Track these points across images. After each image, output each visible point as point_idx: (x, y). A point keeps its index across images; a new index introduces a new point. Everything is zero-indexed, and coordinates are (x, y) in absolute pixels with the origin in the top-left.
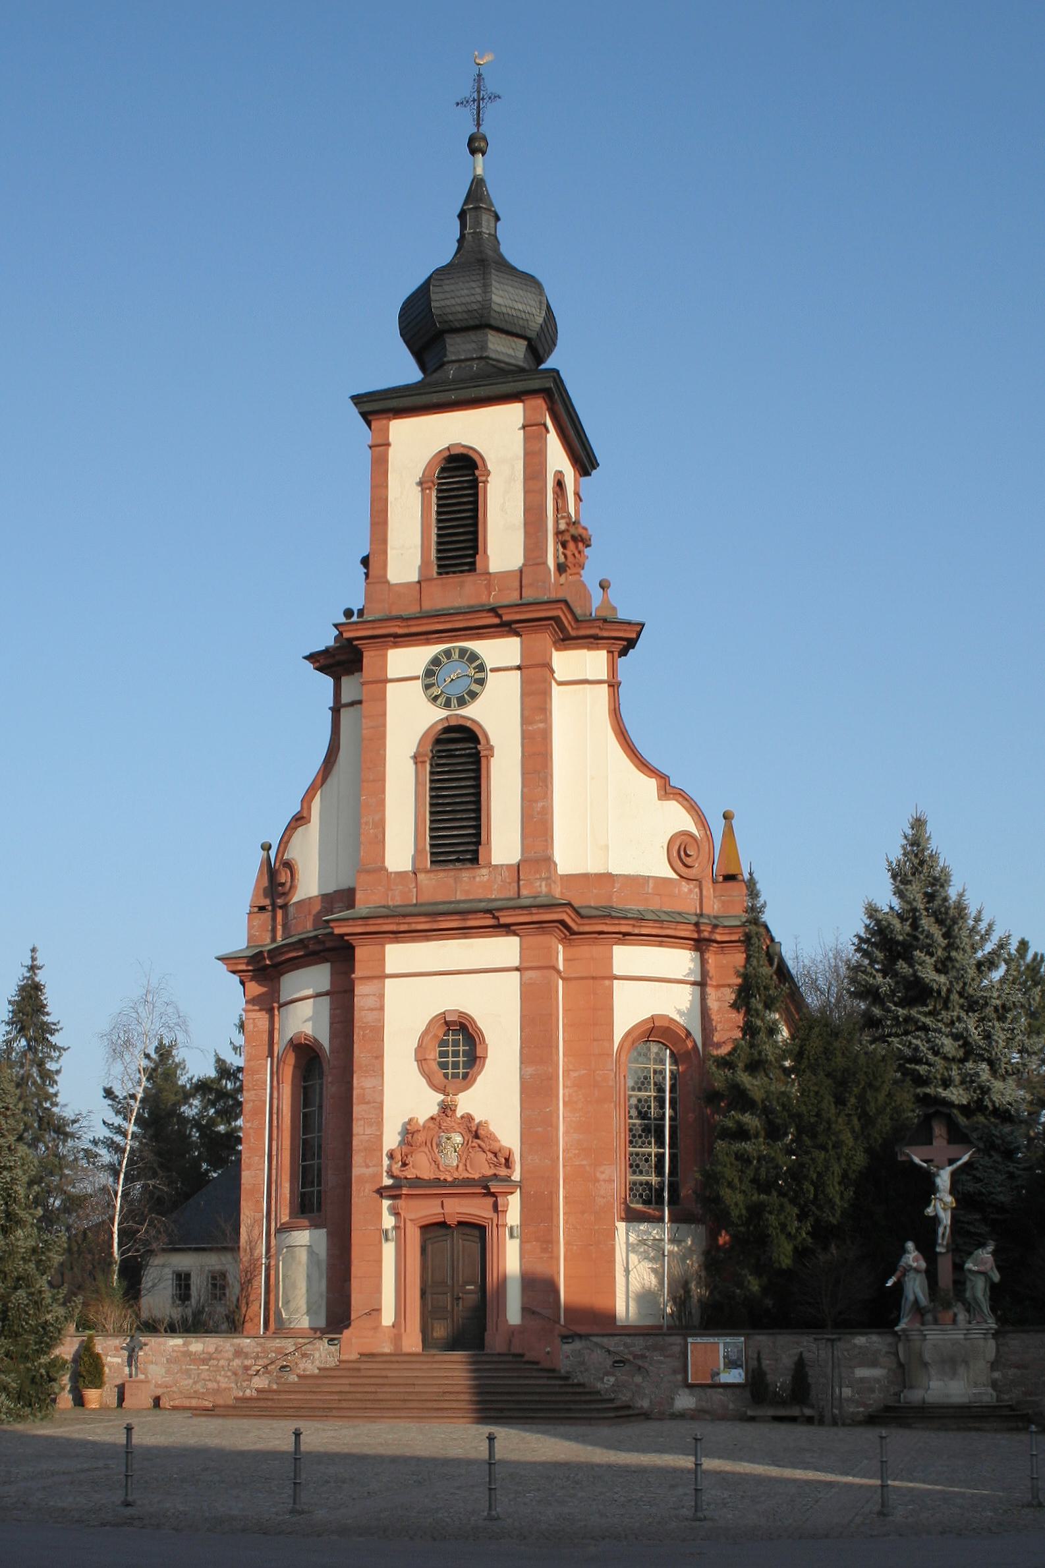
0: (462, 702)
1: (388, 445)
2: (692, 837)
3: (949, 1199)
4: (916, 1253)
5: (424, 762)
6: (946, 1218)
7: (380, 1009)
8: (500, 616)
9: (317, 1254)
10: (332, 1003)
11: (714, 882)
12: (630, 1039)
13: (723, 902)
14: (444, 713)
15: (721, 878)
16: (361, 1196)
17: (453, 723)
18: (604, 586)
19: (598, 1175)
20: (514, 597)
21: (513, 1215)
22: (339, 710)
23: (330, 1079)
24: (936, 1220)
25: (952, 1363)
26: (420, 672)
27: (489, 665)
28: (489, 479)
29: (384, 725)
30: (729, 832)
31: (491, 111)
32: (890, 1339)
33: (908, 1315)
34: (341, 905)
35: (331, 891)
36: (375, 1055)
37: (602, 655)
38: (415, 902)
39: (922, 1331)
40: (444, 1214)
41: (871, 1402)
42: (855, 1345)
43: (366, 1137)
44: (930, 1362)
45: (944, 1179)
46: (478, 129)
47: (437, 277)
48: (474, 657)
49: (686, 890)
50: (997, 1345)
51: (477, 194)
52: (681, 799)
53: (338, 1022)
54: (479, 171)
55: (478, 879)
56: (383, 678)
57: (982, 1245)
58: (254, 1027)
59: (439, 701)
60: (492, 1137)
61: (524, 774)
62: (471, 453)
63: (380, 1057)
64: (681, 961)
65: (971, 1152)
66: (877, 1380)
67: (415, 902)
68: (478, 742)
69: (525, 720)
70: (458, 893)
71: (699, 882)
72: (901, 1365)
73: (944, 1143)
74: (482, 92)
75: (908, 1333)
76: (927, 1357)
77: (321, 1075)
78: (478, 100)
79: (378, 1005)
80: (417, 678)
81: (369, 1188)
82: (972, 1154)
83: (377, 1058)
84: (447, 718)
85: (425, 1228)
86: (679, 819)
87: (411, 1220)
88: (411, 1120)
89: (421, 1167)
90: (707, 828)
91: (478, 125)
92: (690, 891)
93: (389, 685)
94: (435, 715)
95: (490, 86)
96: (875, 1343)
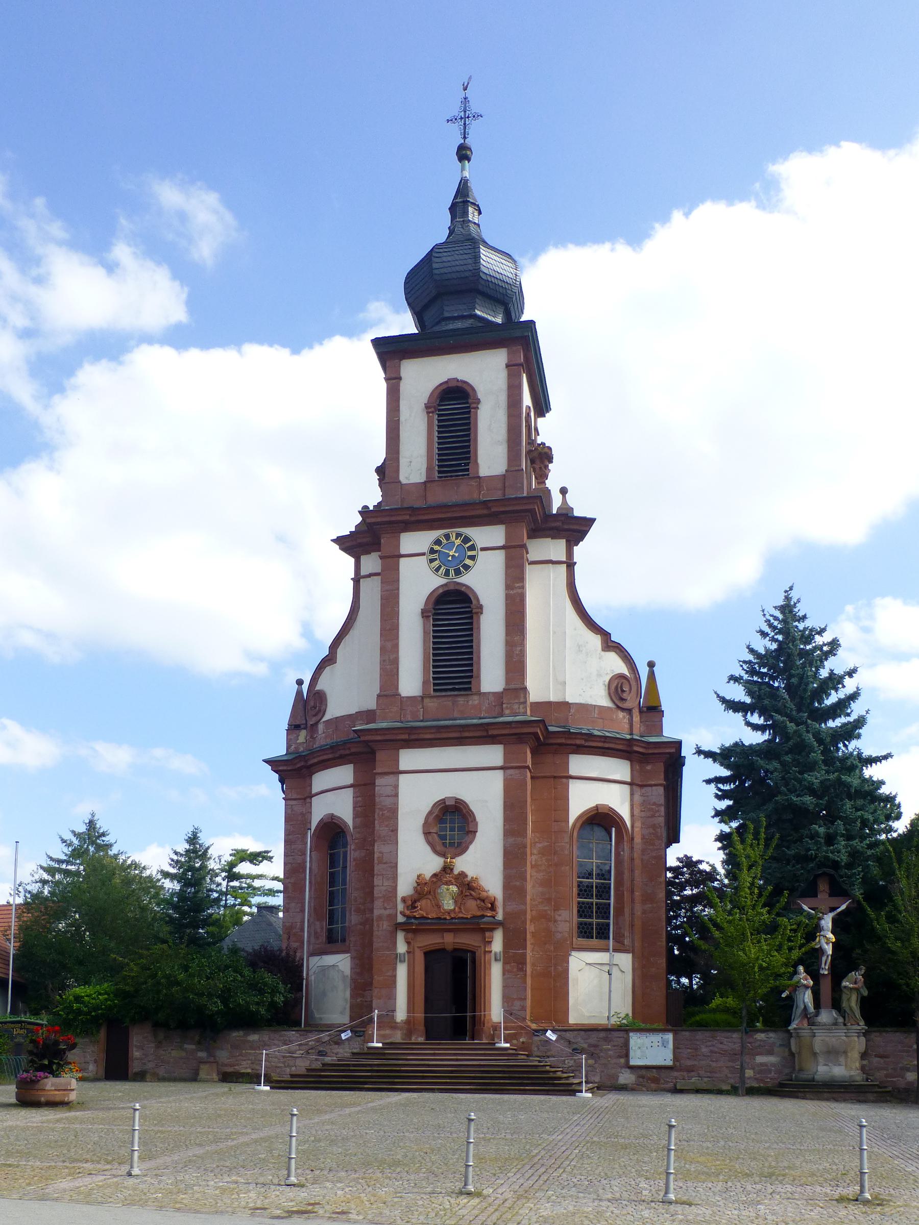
0: (458, 573)
1: (400, 378)
2: (624, 677)
3: (831, 936)
4: (805, 974)
5: (428, 617)
6: (829, 949)
7: (395, 796)
8: (489, 508)
9: (343, 972)
10: (354, 793)
11: (641, 712)
12: (580, 822)
13: (647, 726)
14: (443, 581)
15: (645, 709)
16: (381, 929)
17: (452, 587)
18: (564, 491)
19: (557, 917)
20: (498, 495)
21: (497, 944)
22: (359, 581)
23: (353, 847)
24: (821, 951)
25: (833, 1053)
26: (425, 549)
27: (480, 545)
28: (479, 406)
29: (398, 589)
30: (652, 676)
31: (474, 127)
32: (781, 1035)
33: (798, 1019)
34: (361, 722)
35: (354, 713)
36: (391, 829)
37: (563, 543)
38: (422, 718)
39: (813, 1030)
40: (444, 943)
41: (769, 1080)
42: (756, 1040)
43: (385, 888)
44: (818, 1052)
45: (827, 922)
46: (464, 141)
47: (437, 250)
48: (467, 539)
49: (621, 717)
50: (867, 1041)
51: (463, 190)
52: (618, 651)
53: (360, 807)
54: (466, 174)
55: (470, 703)
56: (396, 554)
57: (856, 969)
58: (292, 811)
59: (440, 572)
60: (479, 889)
61: (507, 626)
62: (464, 386)
63: (395, 830)
64: (620, 769)
65: (848, 902)
66: (773, 1065)
67: (422, 718)
68: (471, 602)
69: (508, 587)
70: (455, 712)
71: (629, 711)
72: (792, 1055)
73: (827, 896)
74: (462, 124)
75: (799, 1031)
76: (817, 1049)
77: (345, 845)
78: (465, 118)
79: (393, 793)
80: (423, 554)
81: (386, 925)
82: (849, 904)
83: (392, 831)
84: (446, 585)
85: (427, 954)
86: (616, 665)
87: (418, 947)
88: (419, 876)
89: (424, 908)
90: (636, 672)
91: (465, 138)
92: (624, 717)
93: (402, 560)
94: (436, 582)
95: (474, 107)
96: (771, 1038)
